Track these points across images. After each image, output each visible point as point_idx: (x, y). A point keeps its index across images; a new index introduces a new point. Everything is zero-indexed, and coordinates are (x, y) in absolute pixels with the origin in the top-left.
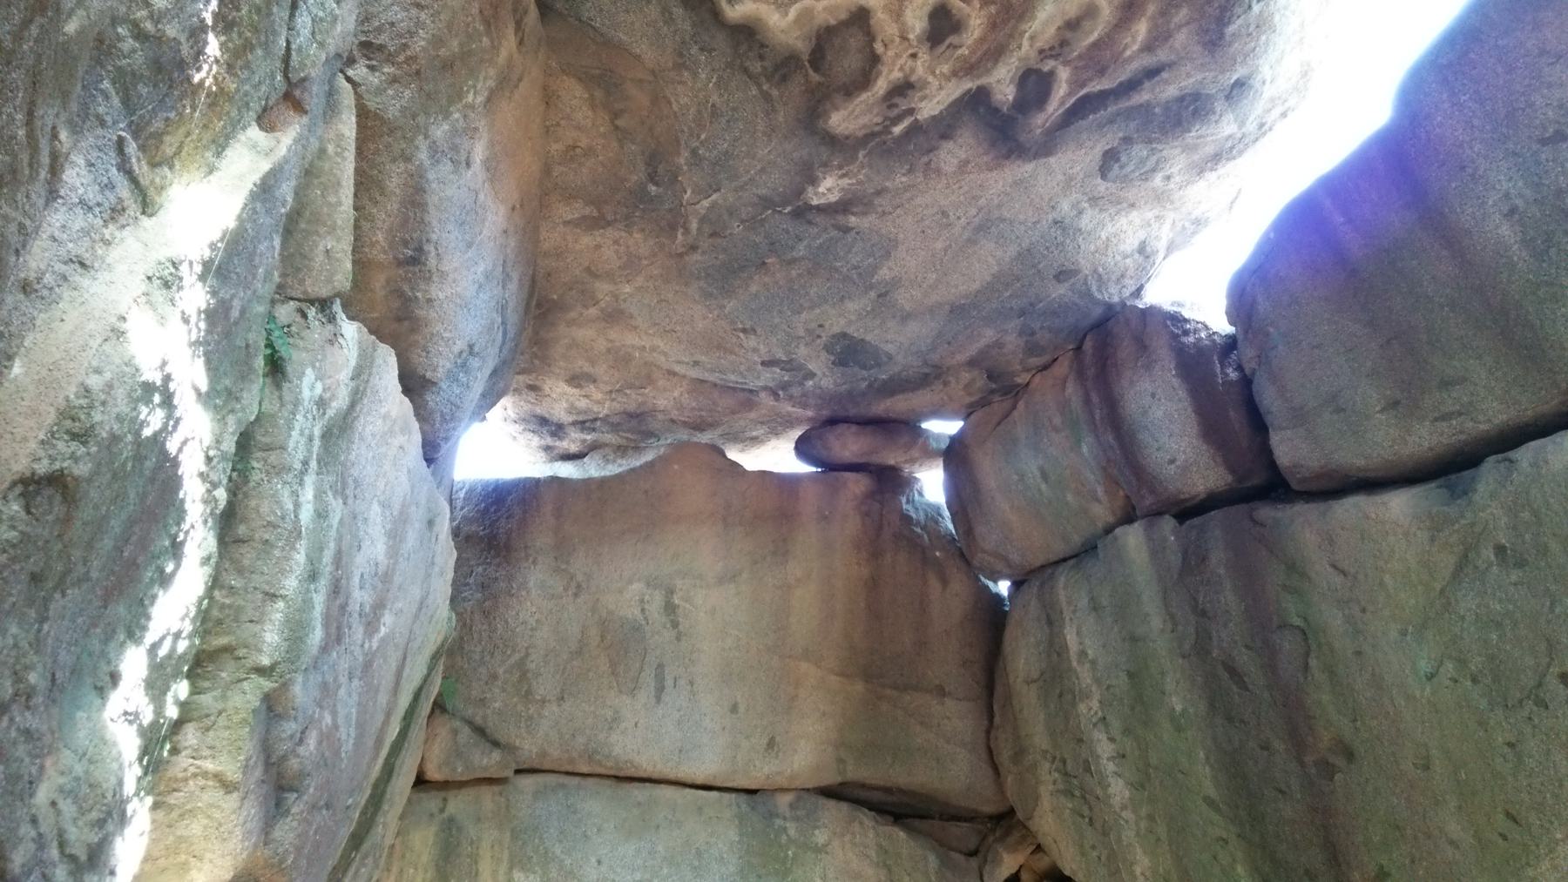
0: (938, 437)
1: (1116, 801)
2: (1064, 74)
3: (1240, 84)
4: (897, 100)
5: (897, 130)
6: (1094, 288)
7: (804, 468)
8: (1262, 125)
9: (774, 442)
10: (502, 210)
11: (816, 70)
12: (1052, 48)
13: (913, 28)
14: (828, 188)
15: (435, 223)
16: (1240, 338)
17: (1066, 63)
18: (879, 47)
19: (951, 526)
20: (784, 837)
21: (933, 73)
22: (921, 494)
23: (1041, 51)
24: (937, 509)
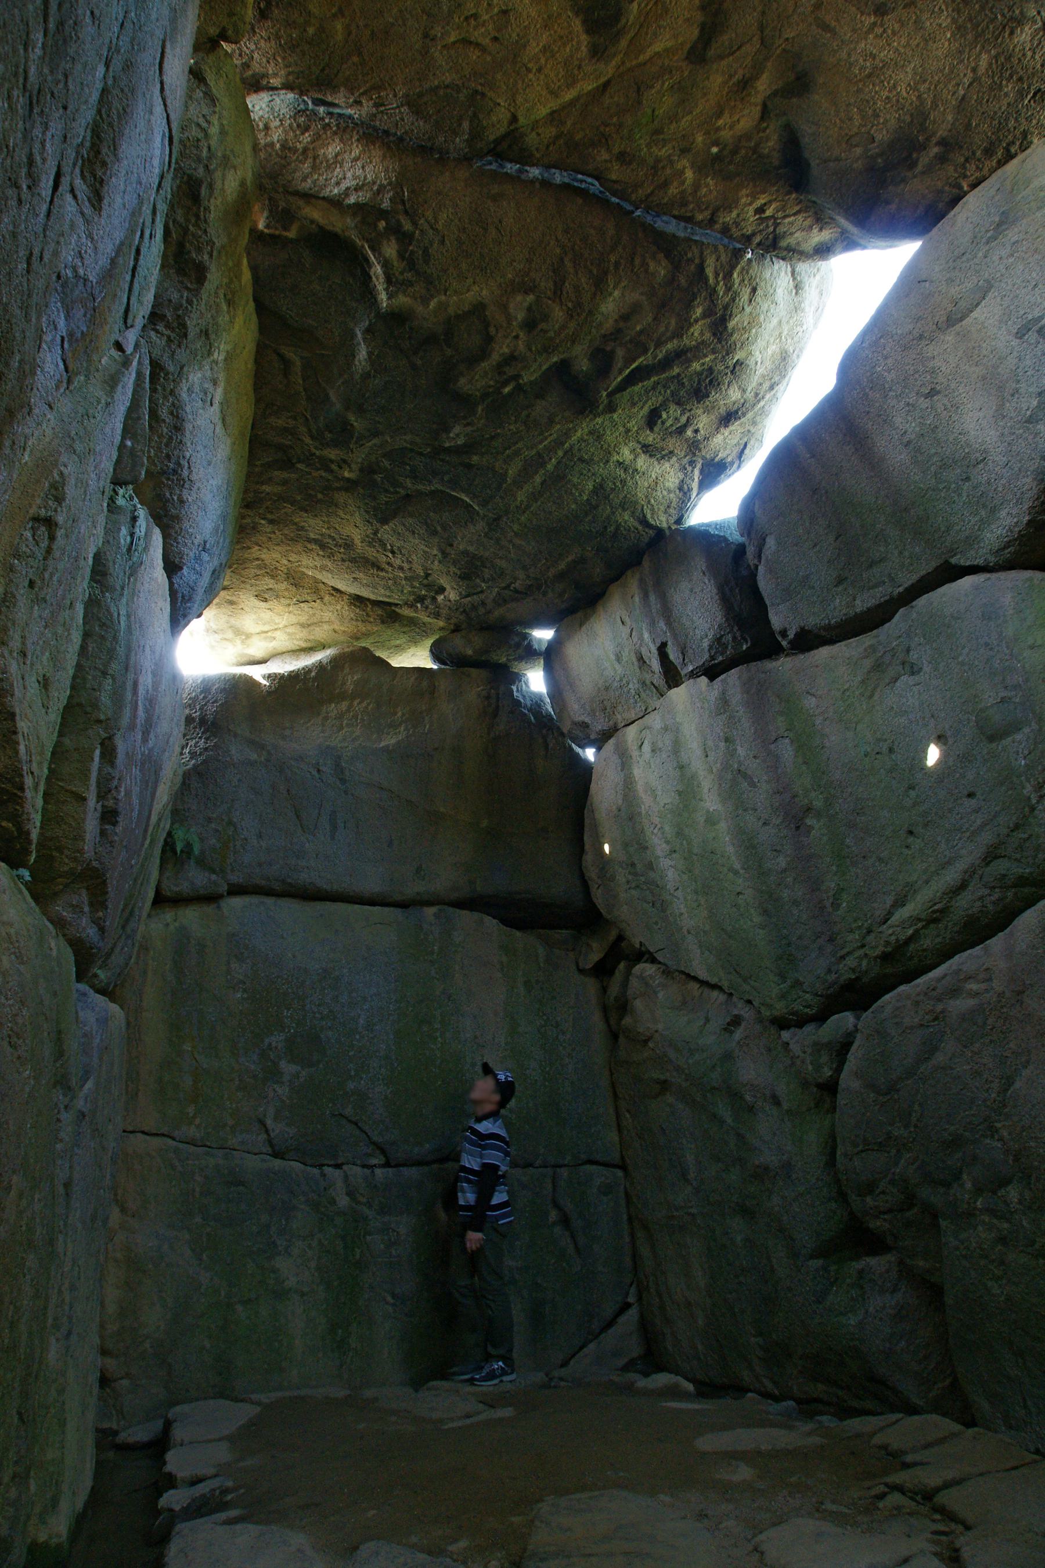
0: (540, 641)
1: (670, 886)
2: (620, 353)
3: (739, 363)
4: (506, 369)
5: (507, 390)
6: (649, 516)
8: (757, 395)
9: (412, 650)
10: (229, 442)
12: (611, 334)
14: (457, 435)
15: (189, 444)
16: (747, 544)
18: (492, 330)
19: (550, 710)
20: (431, 937)
21: (530, 350)
22: (527, 684)
23: (604, 336)
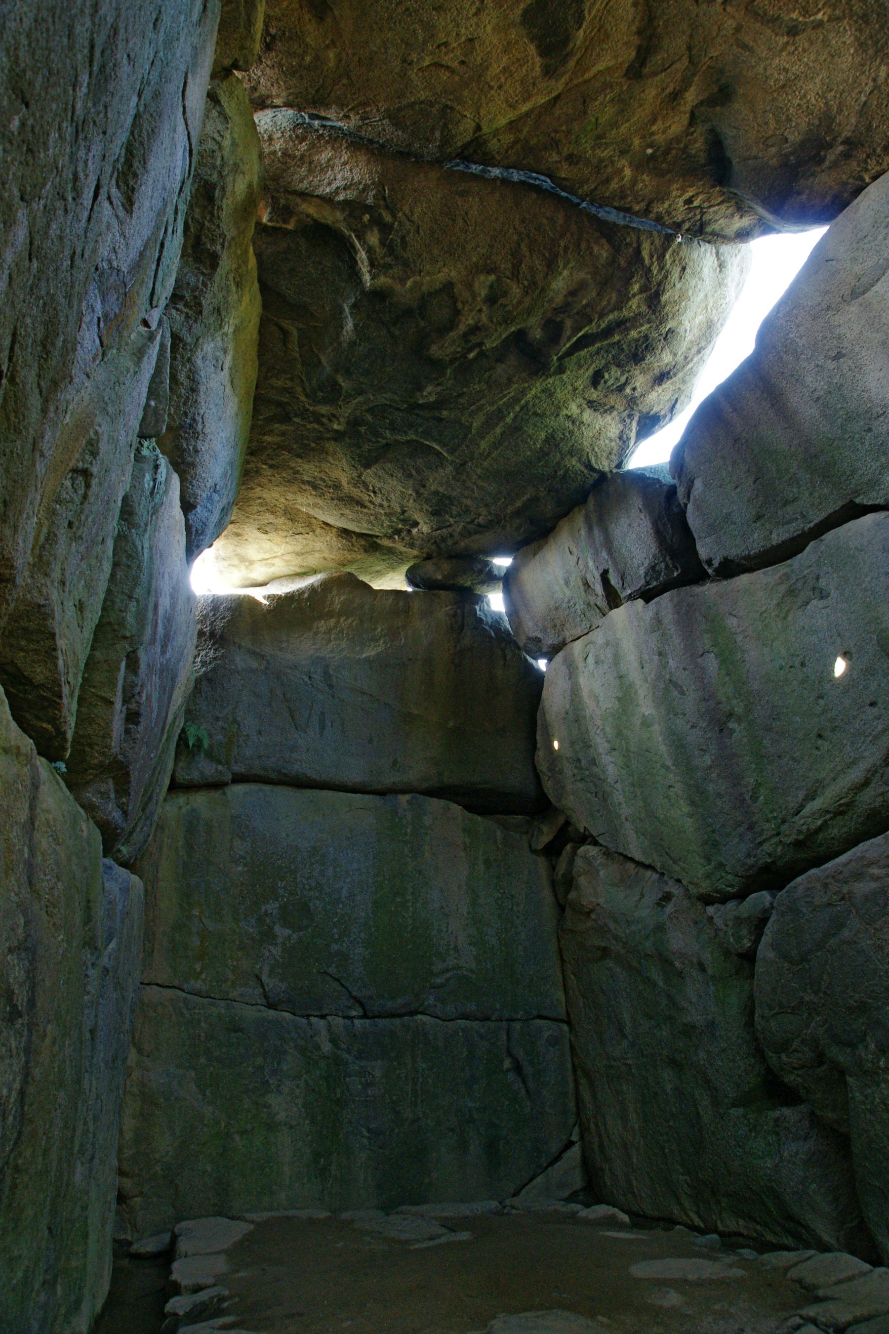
0: (499, 568)
2: (569, 323)
5: (471, 355)
6: (593, 462)
7: (410, 589)
8: (686, 358)
9: (391, 575)
10: (236, 400)
11: (423, 319)
12: (561, 307)
13: (480, 295)
14: (429, 393)
15: (203, 403)
17: (569, 316)
18: (460, 306)
19: (508, 626)
21: (492, 322)
23: (555, 309)
24: (499, 615)
